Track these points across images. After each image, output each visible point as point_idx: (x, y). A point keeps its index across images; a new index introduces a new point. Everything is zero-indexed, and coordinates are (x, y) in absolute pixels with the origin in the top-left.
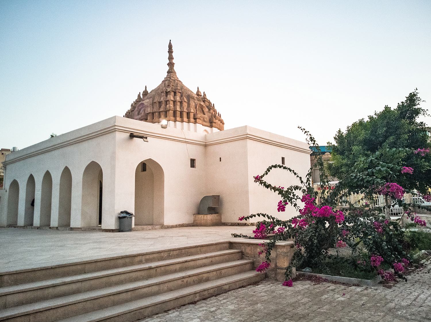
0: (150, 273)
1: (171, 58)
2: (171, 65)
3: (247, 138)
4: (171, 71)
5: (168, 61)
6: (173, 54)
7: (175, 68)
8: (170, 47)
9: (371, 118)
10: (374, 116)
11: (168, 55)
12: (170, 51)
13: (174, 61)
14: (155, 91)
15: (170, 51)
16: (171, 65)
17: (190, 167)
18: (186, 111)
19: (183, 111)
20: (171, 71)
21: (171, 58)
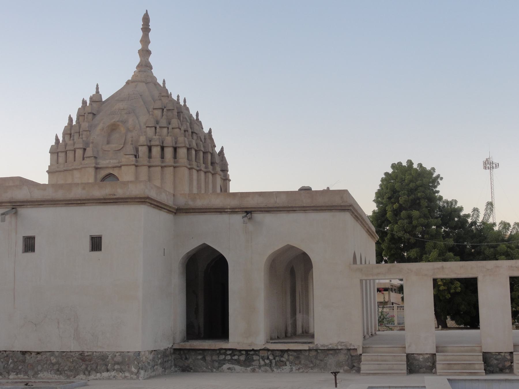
0: (372, 360)
1: (145, 40)
2: (145, 52)
3: (147, 200)
4: (145, 67)
5: (140, 46)
6: (150, 34)
7: (151, 59)
8: (146, 19)
9: (438, 192)
10: (415, 166)
11: (141, 34)
12: (146, 29)
13: (150, 47)
14: (115, 98)
15: (146, 29)
16: (145, 52)
17: (103, 238)
18: (203, 149)
19: (200, 150)
20: (145, 67)
21: (145, 40)
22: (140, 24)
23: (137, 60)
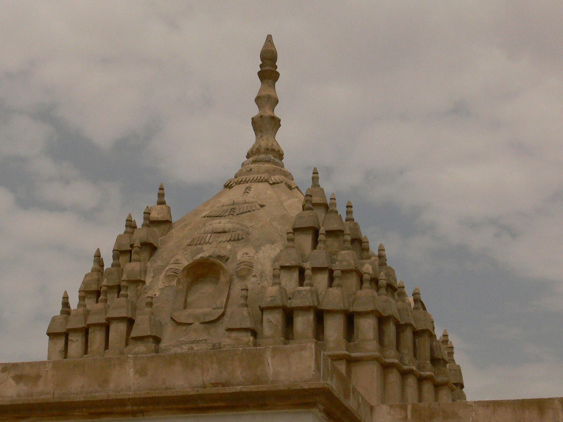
12: (268, 72)
15: (268, 72)
21: (267, 100)
22: (256, 64)
23: (249, 138)
